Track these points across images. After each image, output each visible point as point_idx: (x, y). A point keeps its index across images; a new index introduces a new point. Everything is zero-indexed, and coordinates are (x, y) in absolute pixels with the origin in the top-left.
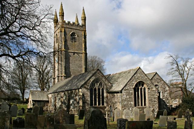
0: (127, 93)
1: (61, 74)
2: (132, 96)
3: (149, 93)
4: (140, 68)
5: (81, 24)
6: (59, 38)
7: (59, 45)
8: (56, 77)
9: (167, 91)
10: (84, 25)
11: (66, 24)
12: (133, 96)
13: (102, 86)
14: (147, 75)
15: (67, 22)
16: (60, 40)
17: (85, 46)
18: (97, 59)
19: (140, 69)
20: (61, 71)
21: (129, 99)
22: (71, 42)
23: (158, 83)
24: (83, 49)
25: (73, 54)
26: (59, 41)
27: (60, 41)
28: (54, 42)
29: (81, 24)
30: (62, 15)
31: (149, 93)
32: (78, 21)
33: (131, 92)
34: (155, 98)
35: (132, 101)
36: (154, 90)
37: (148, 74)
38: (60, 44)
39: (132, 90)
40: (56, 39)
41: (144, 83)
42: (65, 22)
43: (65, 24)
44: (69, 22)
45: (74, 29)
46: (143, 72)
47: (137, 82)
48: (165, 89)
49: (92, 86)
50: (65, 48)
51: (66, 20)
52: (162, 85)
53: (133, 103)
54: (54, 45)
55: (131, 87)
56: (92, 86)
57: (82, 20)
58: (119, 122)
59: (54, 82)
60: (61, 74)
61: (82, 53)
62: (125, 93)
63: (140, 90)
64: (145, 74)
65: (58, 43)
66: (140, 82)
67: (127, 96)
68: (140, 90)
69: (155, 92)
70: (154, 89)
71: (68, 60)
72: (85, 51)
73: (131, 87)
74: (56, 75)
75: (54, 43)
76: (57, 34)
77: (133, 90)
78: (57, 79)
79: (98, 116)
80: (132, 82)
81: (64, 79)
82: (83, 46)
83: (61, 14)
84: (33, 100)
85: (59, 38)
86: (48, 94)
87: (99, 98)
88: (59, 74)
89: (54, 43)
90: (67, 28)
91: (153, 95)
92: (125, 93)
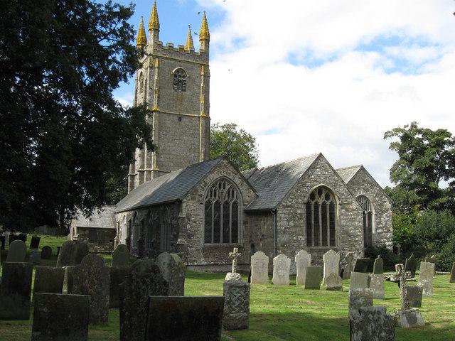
0: (288, 214)
1: (149, 165)
2: (302, 221)
3: (342, 214)
4: (321, 154)
5: (197, 50)
6: (146, 80)
7: (145, 98)
8: (136, 172)
9: (386, 211)
10: (205, 55)
11: (164, 50)
12: (303, 222)
13: (215, 196)
14: (338, 172)
15: (164, 45)
16: (148, 86)
17: (205, 100)
18: (238, 130)
19: (321, 158)
20: (147, 160)
21: (293, 230)
22: (173, 91)
23: (367, 190)
24: (202, 107)
25: (176, 118)
26: (146, 88)
27: (148, 89)
28: (136, 91)
29: (197, 50)
30: (156, 30)
31: (348, 218)
32: (191, 43)
33: (299, 211)
34: (356, 228)
35: (299, 235)
36: (354, 207)
37: (339, 170)
38: (147, 97)
39: (300, 208)
40: (139, 83)
41: (330, 190)
42: (160, 45)
43: (160, 49)
44: (171, 47)
45: (180, 61)
46: (329, 165)
47: (315, 187)
48: (381, 205)
49: (211, 196)
50: (158, 105)
51: (165, 39)
52: (376, 196)
53: (303, 238)
54: (136, 98)
55: (300, 200)
56: (211, 196)
57: (201, 40)
58: (389, 268)
59: (133, 183)
60: (149, 165)
61: (199, 117)
62: (285, 214)
63: (320, 207)
64: (334, 171)
65: (143, 94)
66: (320, 190)
67: (288, 221)
68: (320, 207)
69: (355, 212)
70: (355, 205)
71: (164, 133)
72: (205, 111)
73: (300, 200)
74: (136, 168)
75: (136, 93)
76: (142, 73)
77: (304, 207)
78: (137, 177)
79: (147, 276)
80: (302, 189)
81: (154, 177)
82: (202, 101)
83: (152, 27)
84: (78, 228)
85: (146, 80)
86: (115, 213)
87: (217, 223)
88: (142, 166)
89: (136, 93)
90: (167, 58)
91: (352, 220)
92: (285, 214)
